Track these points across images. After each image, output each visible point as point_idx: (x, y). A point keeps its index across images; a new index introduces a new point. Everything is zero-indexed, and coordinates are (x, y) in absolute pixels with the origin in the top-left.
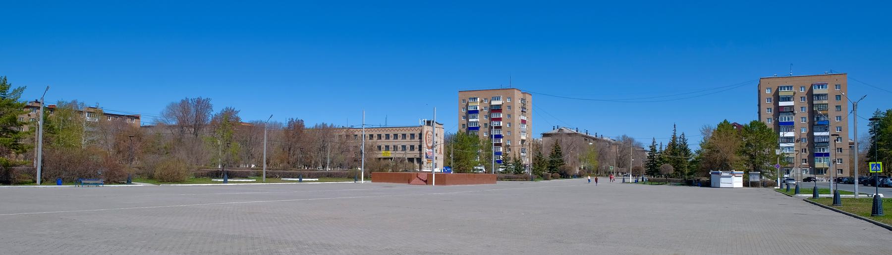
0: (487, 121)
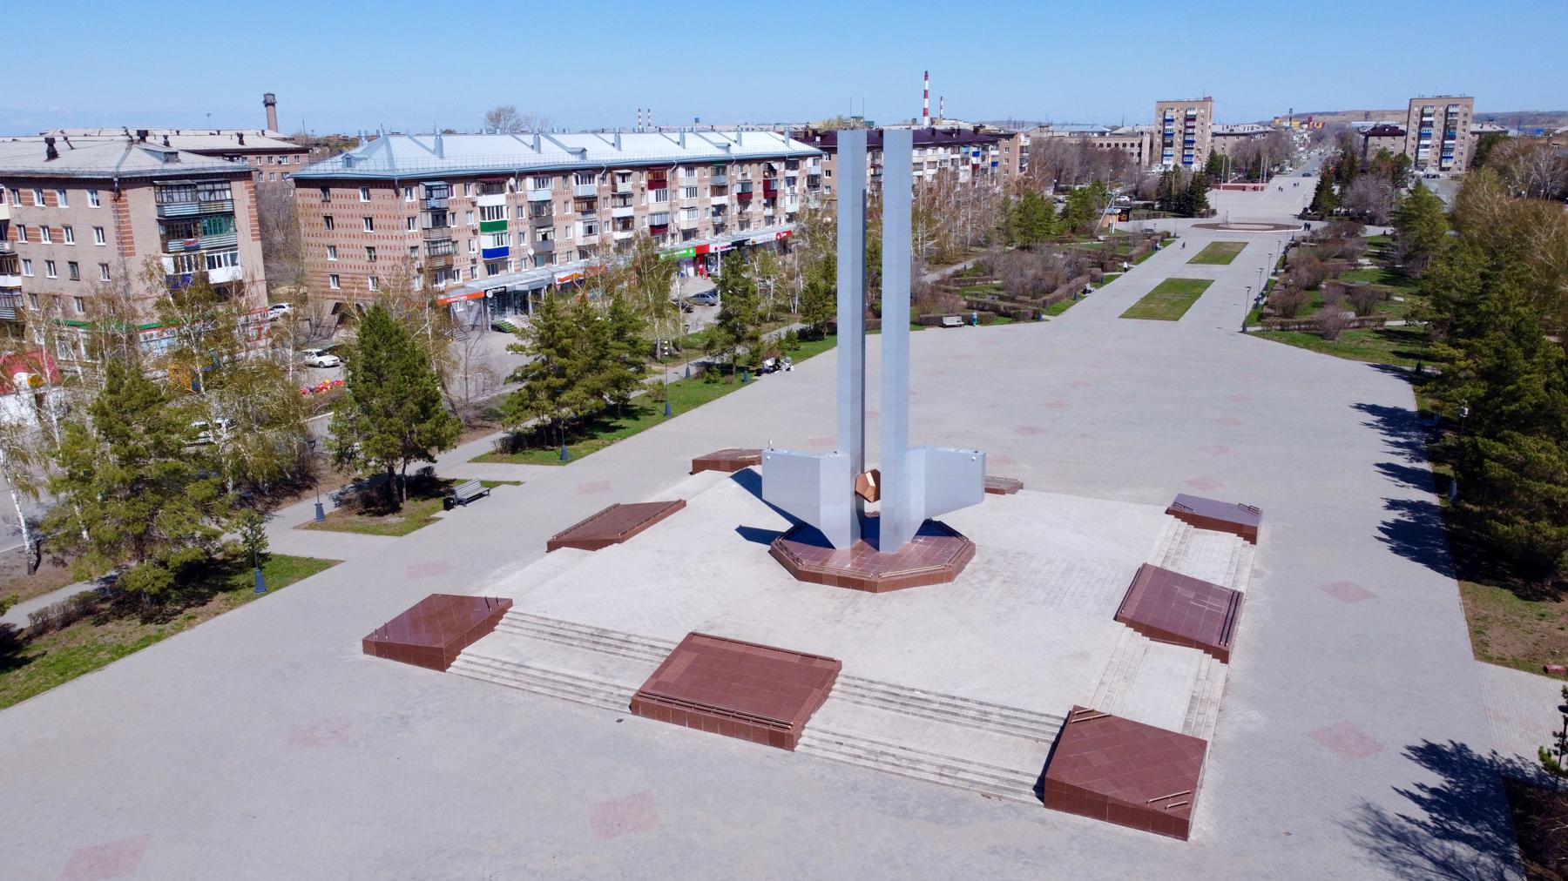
0: (1182, 128)
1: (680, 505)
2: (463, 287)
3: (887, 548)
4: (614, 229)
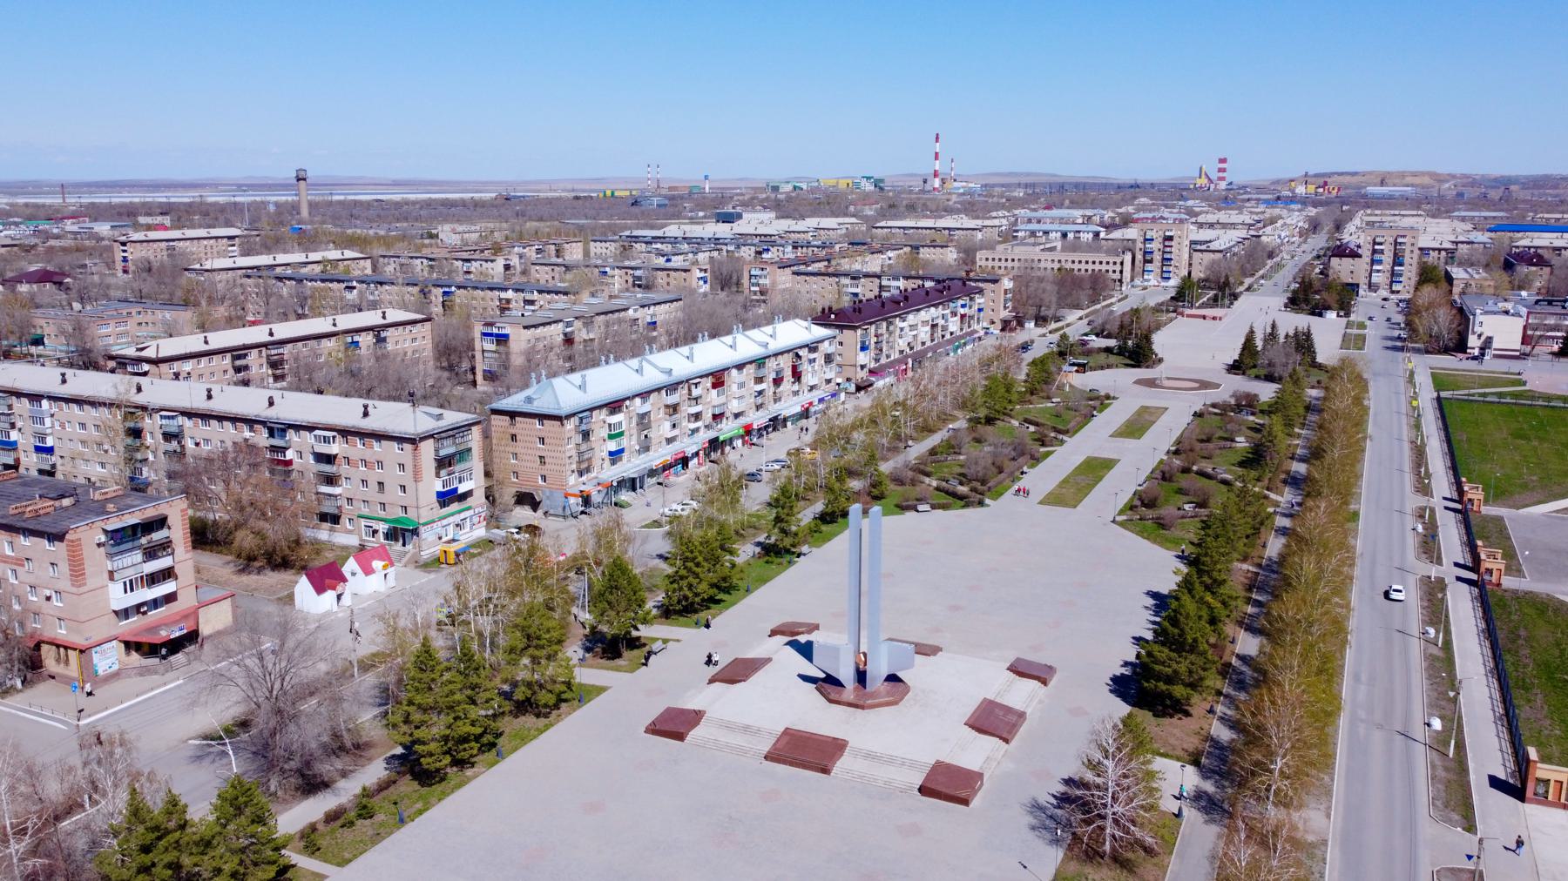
0: (1161, 247)
1: (769, 660)
2: (596, 478)
3: (870, 687)
4: (689, 421)
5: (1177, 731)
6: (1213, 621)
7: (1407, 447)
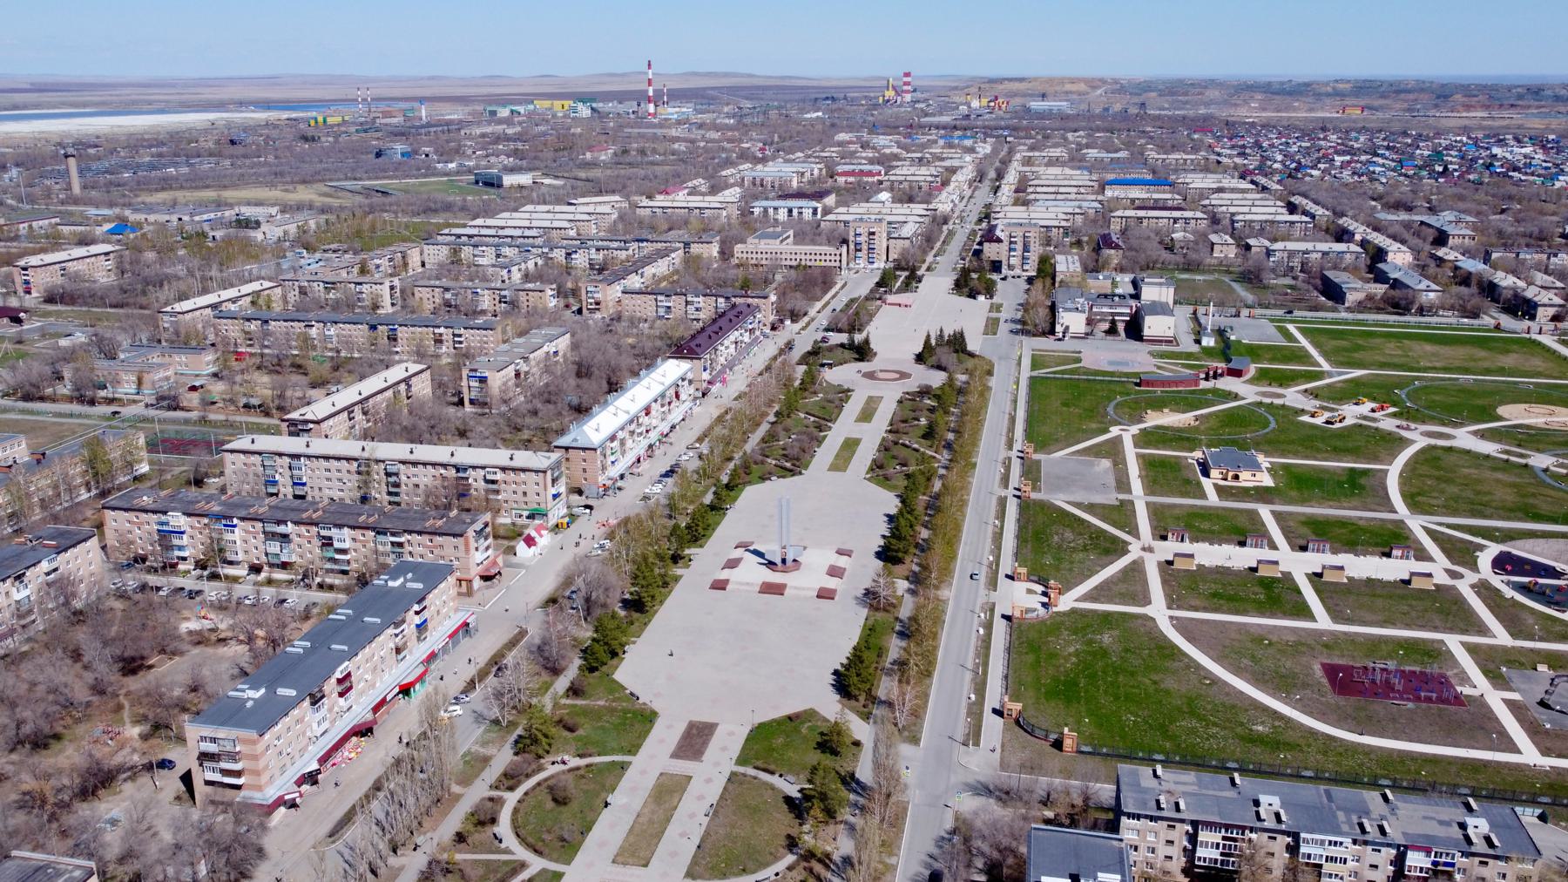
5: (899, 569)
6: (911, 526)
7: (1007, 416)
